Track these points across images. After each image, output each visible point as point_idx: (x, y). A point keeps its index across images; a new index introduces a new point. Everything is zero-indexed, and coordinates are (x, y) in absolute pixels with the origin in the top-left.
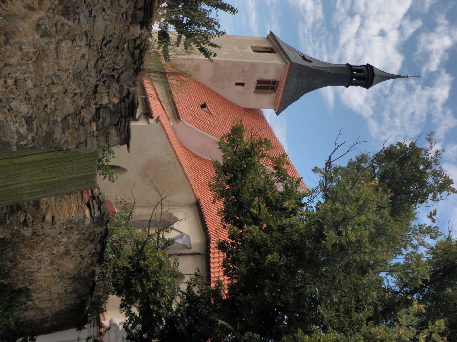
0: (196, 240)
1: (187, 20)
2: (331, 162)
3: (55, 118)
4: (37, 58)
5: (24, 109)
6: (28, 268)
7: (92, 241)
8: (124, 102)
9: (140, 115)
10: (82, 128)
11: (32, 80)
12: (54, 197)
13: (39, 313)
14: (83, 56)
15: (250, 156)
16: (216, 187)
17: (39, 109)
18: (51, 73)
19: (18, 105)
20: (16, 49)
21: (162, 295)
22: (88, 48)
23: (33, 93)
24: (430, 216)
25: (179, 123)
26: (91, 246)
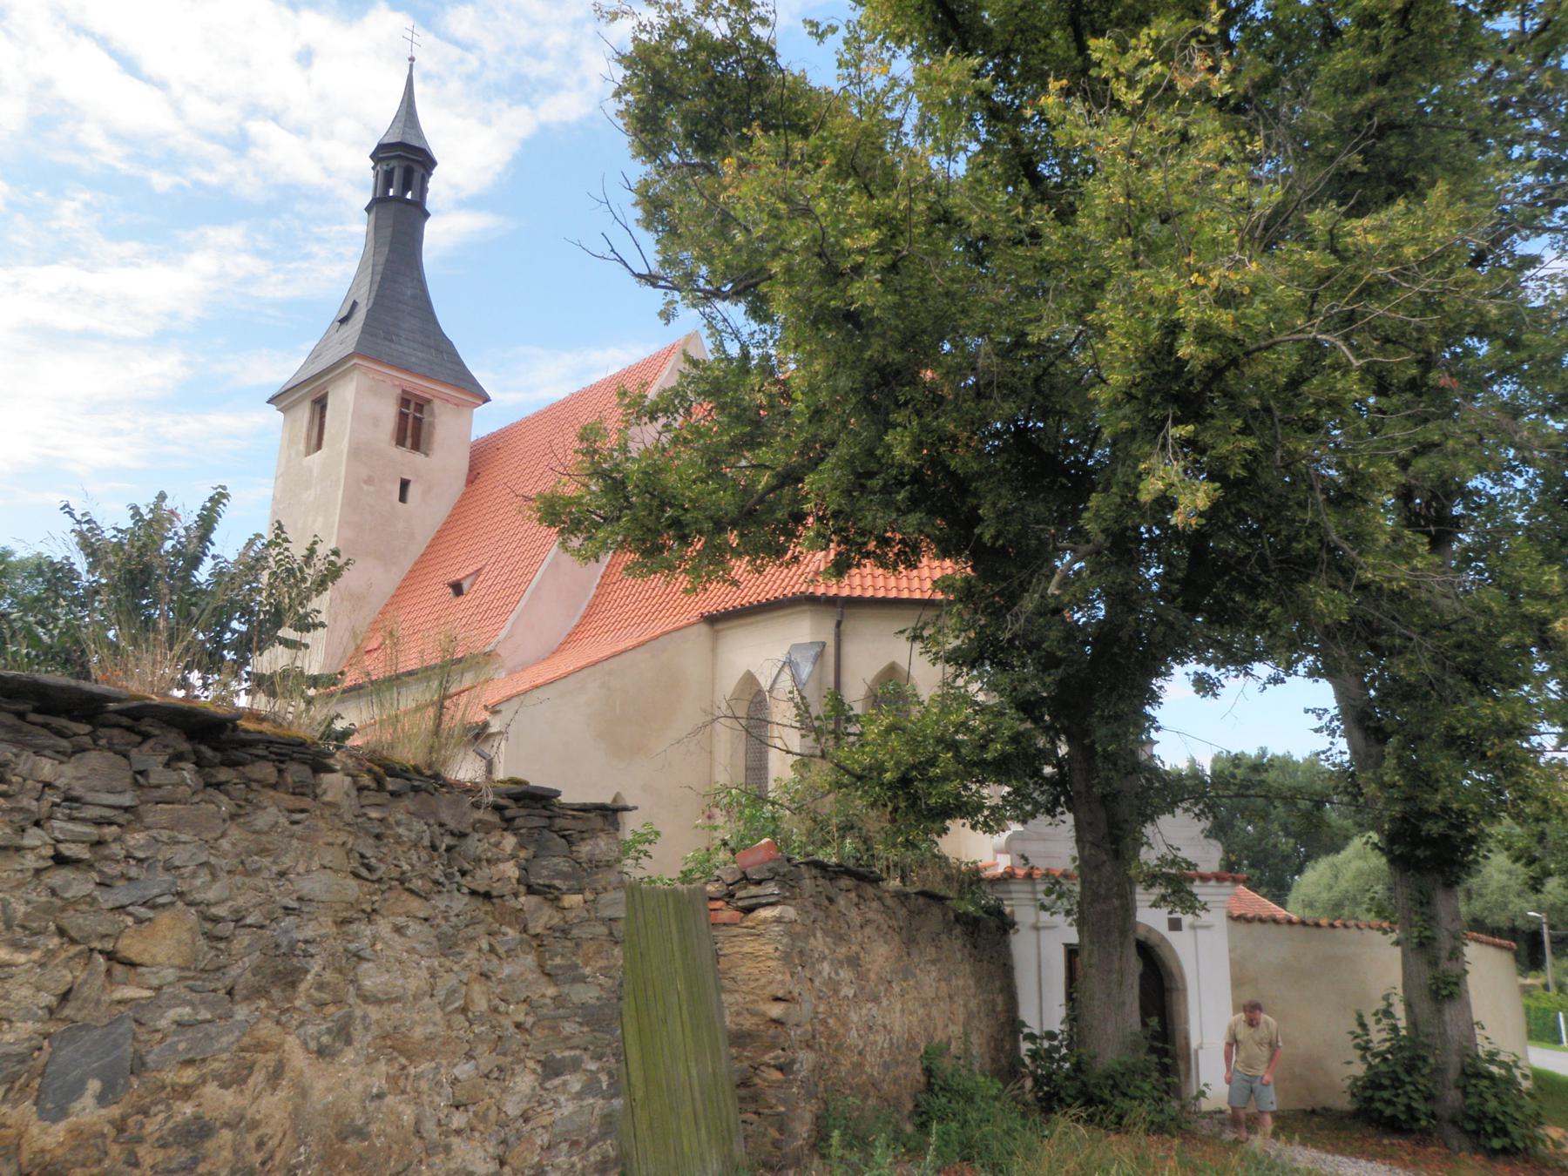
0: (804, 630)
1: (238, 620)
2: (650, 275)
3: (548, 1001)
4: (401, 1052)
5: (524, 1082)
6: (881, 1056)
7: (831, 900)
8: (513, 819)
10: (575, 932)
11: (455, 1065)
12: (723, 996)
13: (975, 1023)
14: (398, 930)
15: (623, 483)
16: (700, 577)
17: (526, 1045)
18: (438, 1016)
19: (516, 1098)
20: (378, 1109)
21: (963, 726)
22: (378, 918)
23: (487, 1059)
24: (821, 36)
26: (841, 902)
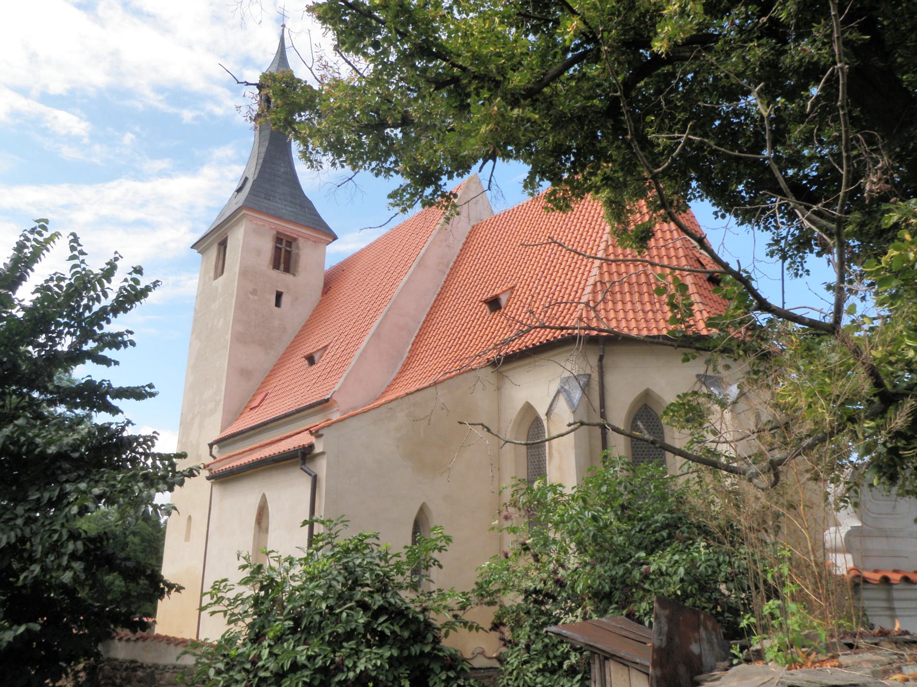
9: (306, 471)
25: (335, 402)
